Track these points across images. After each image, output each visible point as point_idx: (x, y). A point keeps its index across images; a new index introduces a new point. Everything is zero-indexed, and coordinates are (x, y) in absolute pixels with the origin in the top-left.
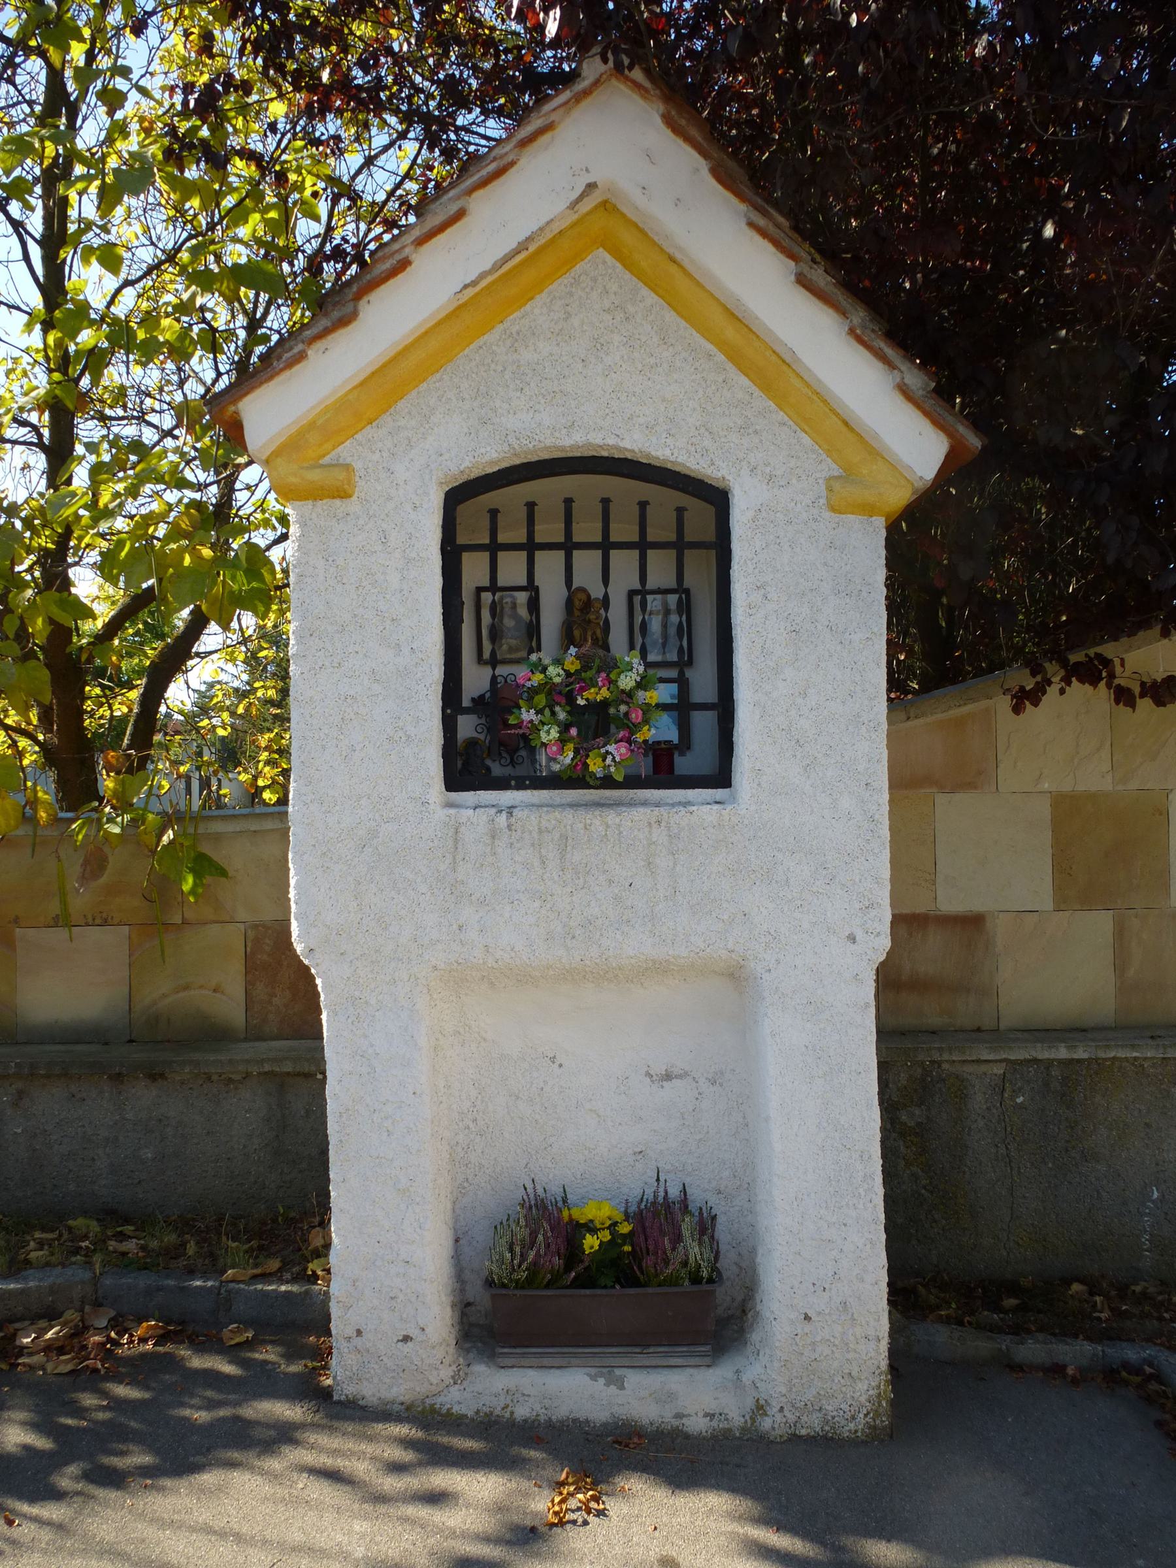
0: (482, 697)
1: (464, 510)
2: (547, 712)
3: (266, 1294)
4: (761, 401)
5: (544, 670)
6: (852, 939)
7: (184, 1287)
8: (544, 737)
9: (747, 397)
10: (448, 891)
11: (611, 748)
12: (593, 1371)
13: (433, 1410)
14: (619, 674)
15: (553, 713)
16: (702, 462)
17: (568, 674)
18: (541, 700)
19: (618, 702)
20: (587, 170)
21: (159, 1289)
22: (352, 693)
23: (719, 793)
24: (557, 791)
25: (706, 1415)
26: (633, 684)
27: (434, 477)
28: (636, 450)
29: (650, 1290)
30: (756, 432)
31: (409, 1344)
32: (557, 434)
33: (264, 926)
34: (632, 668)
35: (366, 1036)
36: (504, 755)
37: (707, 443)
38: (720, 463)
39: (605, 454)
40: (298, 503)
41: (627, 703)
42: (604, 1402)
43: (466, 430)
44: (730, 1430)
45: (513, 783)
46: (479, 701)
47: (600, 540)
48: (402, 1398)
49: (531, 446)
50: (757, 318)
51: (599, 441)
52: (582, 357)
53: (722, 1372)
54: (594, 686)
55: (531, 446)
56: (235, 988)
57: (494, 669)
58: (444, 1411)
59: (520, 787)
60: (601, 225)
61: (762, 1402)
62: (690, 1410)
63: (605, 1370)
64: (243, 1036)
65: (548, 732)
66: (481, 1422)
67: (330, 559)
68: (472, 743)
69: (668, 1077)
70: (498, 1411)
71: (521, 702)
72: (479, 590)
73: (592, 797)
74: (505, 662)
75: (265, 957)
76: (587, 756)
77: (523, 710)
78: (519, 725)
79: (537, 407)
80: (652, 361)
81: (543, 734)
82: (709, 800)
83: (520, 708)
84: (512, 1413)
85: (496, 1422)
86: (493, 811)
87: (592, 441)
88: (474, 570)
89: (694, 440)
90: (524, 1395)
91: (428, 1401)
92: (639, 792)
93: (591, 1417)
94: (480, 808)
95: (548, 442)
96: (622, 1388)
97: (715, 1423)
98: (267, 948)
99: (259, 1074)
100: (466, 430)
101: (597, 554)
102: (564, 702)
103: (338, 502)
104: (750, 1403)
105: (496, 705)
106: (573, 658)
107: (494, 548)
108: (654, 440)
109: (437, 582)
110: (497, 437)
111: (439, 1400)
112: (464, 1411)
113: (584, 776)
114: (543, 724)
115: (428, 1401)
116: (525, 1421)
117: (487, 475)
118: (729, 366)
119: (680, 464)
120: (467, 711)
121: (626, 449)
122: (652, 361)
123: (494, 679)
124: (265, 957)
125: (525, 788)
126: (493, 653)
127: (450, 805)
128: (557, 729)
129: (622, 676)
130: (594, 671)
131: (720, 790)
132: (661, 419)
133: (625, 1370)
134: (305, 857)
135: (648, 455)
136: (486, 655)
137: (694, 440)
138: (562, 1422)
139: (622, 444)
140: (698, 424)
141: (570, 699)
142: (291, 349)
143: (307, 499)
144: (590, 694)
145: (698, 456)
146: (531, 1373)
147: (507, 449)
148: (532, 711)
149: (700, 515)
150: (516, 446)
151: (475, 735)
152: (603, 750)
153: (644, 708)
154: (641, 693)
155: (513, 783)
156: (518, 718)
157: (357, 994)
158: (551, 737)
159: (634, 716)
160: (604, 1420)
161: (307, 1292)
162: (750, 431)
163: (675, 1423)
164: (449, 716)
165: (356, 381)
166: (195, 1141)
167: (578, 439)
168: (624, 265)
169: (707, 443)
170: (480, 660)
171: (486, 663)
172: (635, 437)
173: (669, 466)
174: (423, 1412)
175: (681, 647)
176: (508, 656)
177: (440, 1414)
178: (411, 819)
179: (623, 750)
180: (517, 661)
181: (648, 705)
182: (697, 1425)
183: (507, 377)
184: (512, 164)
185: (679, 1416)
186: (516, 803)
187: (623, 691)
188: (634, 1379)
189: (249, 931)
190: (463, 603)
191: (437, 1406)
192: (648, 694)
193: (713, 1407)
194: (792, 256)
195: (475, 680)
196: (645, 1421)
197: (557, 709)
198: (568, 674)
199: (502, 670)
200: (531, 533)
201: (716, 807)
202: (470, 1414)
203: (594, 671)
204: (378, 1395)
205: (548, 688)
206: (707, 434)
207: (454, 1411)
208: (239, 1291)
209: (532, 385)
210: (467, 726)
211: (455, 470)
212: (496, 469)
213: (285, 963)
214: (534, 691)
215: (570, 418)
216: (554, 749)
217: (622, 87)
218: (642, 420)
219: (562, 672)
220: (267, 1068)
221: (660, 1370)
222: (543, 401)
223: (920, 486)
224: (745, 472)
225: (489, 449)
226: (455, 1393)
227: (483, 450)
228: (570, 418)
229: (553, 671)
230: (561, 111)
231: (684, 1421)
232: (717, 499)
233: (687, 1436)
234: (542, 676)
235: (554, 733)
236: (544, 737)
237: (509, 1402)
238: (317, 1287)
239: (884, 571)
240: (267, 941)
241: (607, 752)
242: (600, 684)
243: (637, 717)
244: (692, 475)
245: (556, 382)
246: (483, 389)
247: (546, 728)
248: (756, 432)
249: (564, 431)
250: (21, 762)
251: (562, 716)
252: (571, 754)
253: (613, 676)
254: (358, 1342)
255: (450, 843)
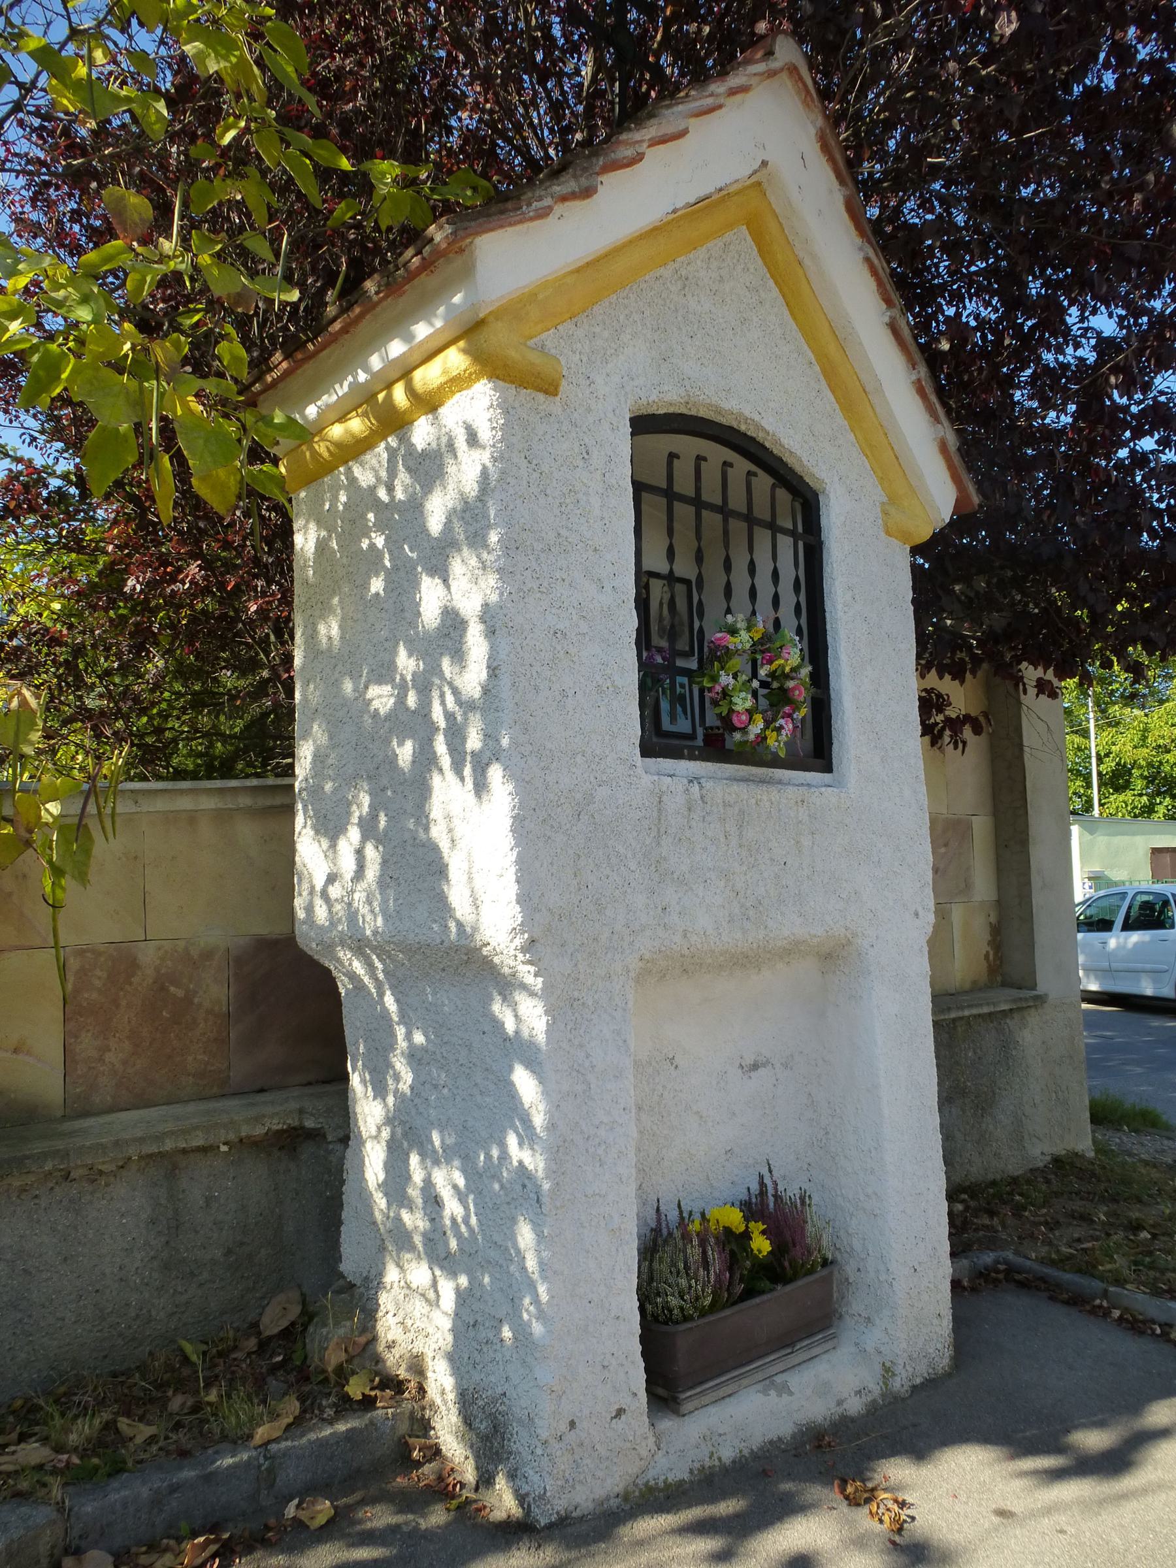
3: (323, 1443)
4: (840, 420)
6: (917, 915)
7: (211, 1473)
10: (653, 868)
12: (759, 1386)
13: (650, 1489)
21: (174, 1489)
22: (561, 626)
29: (800, 1283)
31: (623, 1417)
33: (93, 951)
35: (581, 1046)
40: (501, 383)
42: (784, 1414)
44: (874, 1401)
48: (616, 1490)
50: (861, 344)
53: (844, 1353)
56: (48, 1040)
58: (661, 1485)
60: (747, 208)
61: (888, 1364)
62: (845, 1395)
63: (767, 1382)
64: (59, 1113)
66: (700, 1481)
67: (535, 462)
69: (755, 1067)
70: (708, 1463)
73: (741, 773)
75: (95, 995)
84: (720, 1459)
85: (712, 1475)
90: (720, 1435)
91: (640, 1482)
94: (680, 774)
96: (791, 1393)
98: (98, 983)
99: (141, 1158)
103: (541, 397)
104: (878, 1369)
111: (651, 1474)
115: (640, 1482)
116: (734, 1462)
124: (95, 995)
133: (785, 1374)
134: (526, 823)
135: (777, 442)
138: (761, 1448)
143: (512, 382)
146: (712, 1410)
157: (576, 994)
160: (790, 1431)
161: (372, 1423)
163: (840, 1410)
165: (573, 267)
166: (45, 1276)
168: (759, 250)
174: (642, 1495)
177: (660, 1490)
178: (622, 783)
182: (855, 1406)
184: (720, 107)
185: (840, 1403)
188: (795, 1380)
189: (72, 960)
191: (652, 1483)
194: (888, 302)
196: (820, 1419)
204: (592, 1496)
207: (670, 1480)
208: (285, 1453)
213: (124, 1003)
217: (789, 83)
220: (154, 1149)
221: (804, 1366)
226: (662, 1461)
230: (757, 78)
233: (853, 1420)
237: (711, 1449)
238: (380, 1412)
239: (911, 593)
240: (98, 973)
254: (571, 1437)
255: (655, 814)
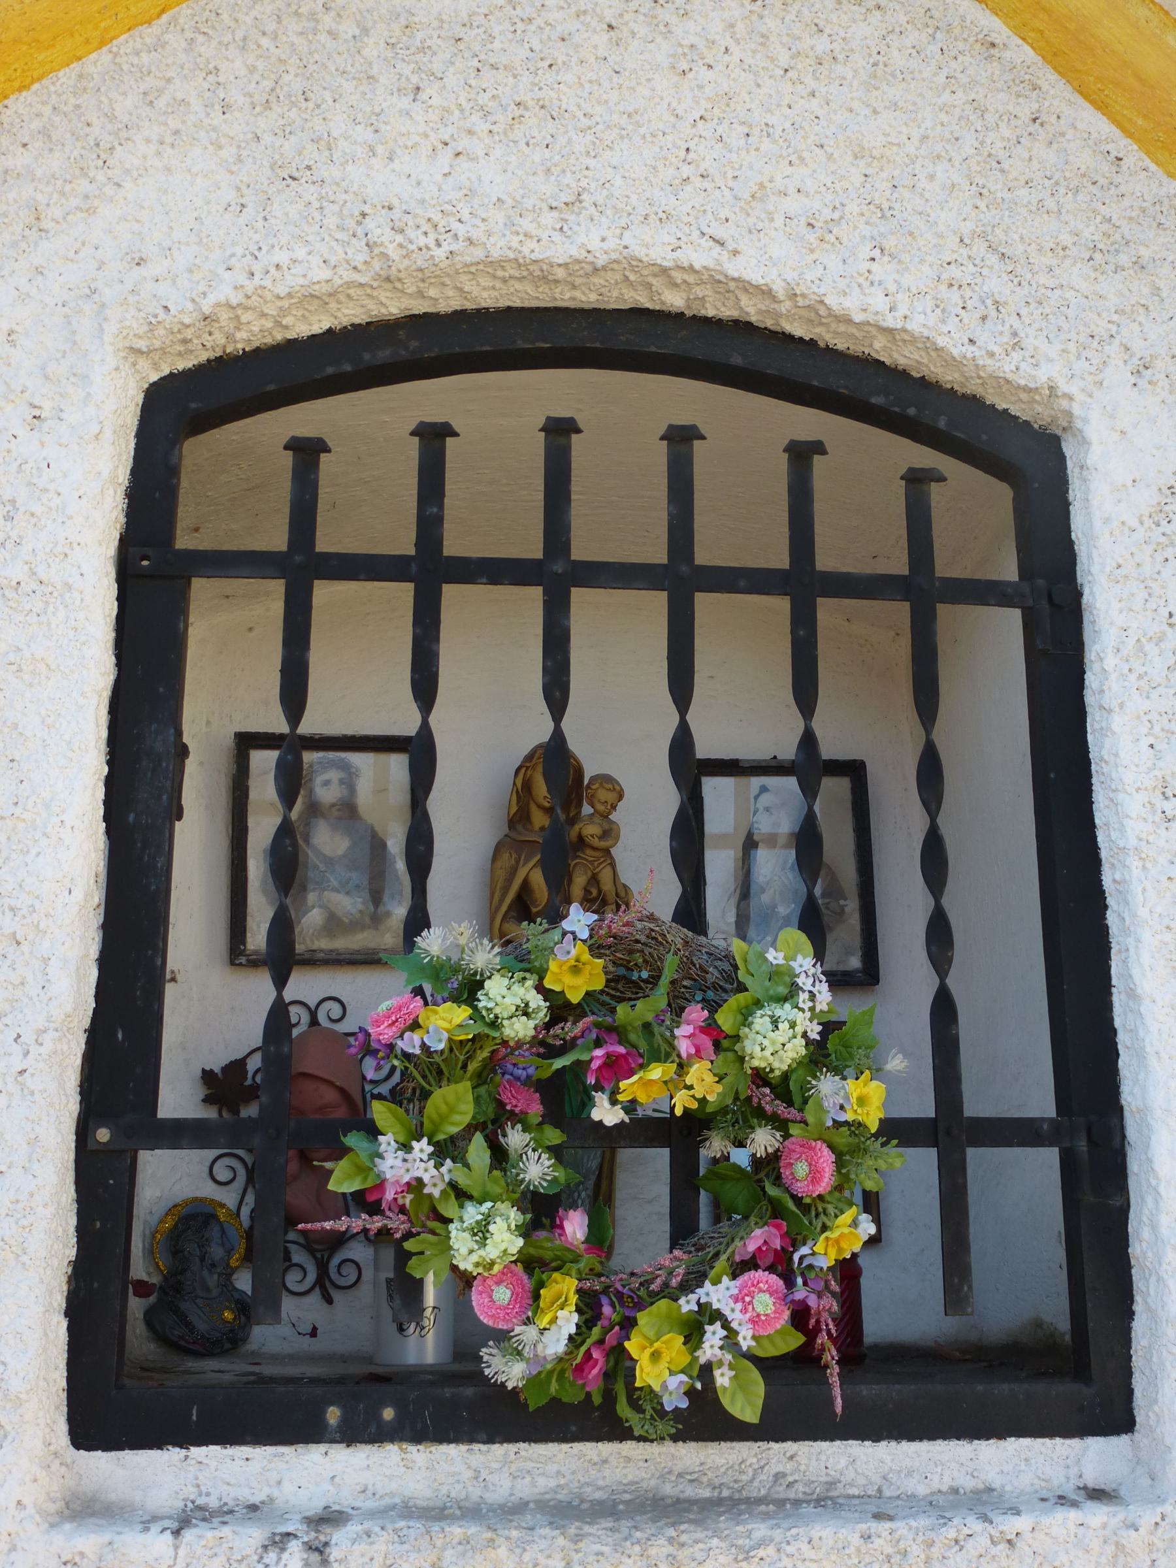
0: (237, 1067)
1: (200, 454)
2: (478, 1151)
5: (469, 989)
8: (464, 1251)
9: (1106, 167)
11: (719, 1294)
14: (746, 1015)
15: (500, 1156)
16: (983, 338)
17: (560, 1009)
18: (455, 1104)
19: (742, 1114)
23: (1093, 1457)
24: (499, 1450)
26: (797, 1049)
27: (111, 328)
28: (779, 288)
30: (1140, 266)
32: (526, 224)
34: (794, 989)
36: (298, 1256)
37: (996, 284)
38: (1044, 347)
39: (674, 301)
41: (781, 1125)
43: (230, 196)
45: (333, 1415)
46: (224, 1085)
47: (662, 558)
49: (440, 253)
51: (661, 254)
52: (609, 17)
54: (657, 1056)
55: (440, 253)
57: (280, 982)
59: (359, 1431)
65: (481, 1232)
68: (192, 1222)
71: (380, 1112)
72: (247, 742)
73: (632, 1474)
74: (312, 961)
76: (628, 1324)
77: (387, 1142)
78: (367, 1201)
79: (463, 143)
80: (821, 45)
81: (460, 1240)
82: (1069, 1490)
83: (373, 1132)
86: (249, 1538)
87: (640, 252)
88: (226, 682)
89: (955, 272)
95: (498, 248)
100: (230, 196)
101: (653, 606)
102: (535, 1111)
105: (287, 1107)
106: (579, 951)
107: (302, 567)
108: (833, 262)
109: (93, 669)
110: (331, 221)
113: (609, 1397)
114: (461, 1194)
117: (291, 345)
118: (1048, 77)
119: (913, 340)
120: (179, 1134)
121: (746, 286)
122: (821, 45)
123: (278, 1015)
125: (378, 1435)
126: (282, 926)
127: (83, 1509)
128: (515, 1216)
129: (761, 1021)
130: (659, 998)
131: (1095, 1444)
132: (853, 208)
135: (816, 310)
136: (257, 938)
137: (955, 272)
139: (734, 268)
140: (966, 228)
141: (562, 1099)
144: (647, 1086)
145: (971, 318)
147: (360, 258)
148: (422, 1148)
150: (393, 252)
151: (208, 1190)
152: (687, 1304)
153: (843, 1138)
154: (827, 1086)
155: (333, 1415)
156: (364, 1170)
158: (492, 1252)
159: (802, 1169)
162: (1124, 259)
164: (106, 1151)
167: (595, 244)
169: (996, 284)
170: (236, 951)
171: (254, 963)
172: (775, 251)
173: (879, 349)
176: (324, 944)
179: (764, 1303)
180: (368, 960)
181: (856, 1127)
183: (370, 52)
186: (344, 1499)
187: (760, 1077)
190: (184, 752)
192: (853, 1087)
195: (210, 1015)
197: (515, 1138)
198: (560, 1009)
199: (305, 986)
200: (429, 526)
201: (1097, 1515)
203: (659, 998)
205: (482, 1057)
206: (993, 259)
209: (451, 81)
210: (168, 1179)
211: (182, 309)
212: (319, 324)
214: (432, 1069)
215: (568, 179)
216: (503, 1294)
218: (792, 205)
219: (536, 1001)
222: (482, 127)
224: (1118, 374)
225: (300, 253)
227: (282, 257)
228: (568, 179)
229: (504, 994)
232: (1026, 461)
234: (460, 1014)
235: (505, 1238)
236: (464, 1251)
241: (708, 1314)
242: (684, 1047)
243: (815, 1176)
244: (949, 378)
245: (526, 79)
246: (293, 83)
247: (472, 1213)
248: (1140, 266)
249: (549, 218)
251: (537, 1170)
252: (569, 1321)
253: (725, 1019)
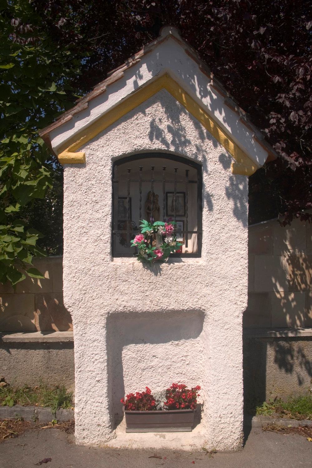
20: (162, 65)
25: (190, 445)
85: (127, 449)
90: (135, 441)
92: (38, 320)
93: (156, 447)
97: (193, 447)
112: (117, 447)
142: (67, 116)
149: (193, 171)
175: (164, 212)
185: (182, 446)
193: (192, 443)
196: (172, 448)
202: (119, 447)
207: (114, 446)
223: (260, 167)
231: (184, 447)
250: (298, 213)
